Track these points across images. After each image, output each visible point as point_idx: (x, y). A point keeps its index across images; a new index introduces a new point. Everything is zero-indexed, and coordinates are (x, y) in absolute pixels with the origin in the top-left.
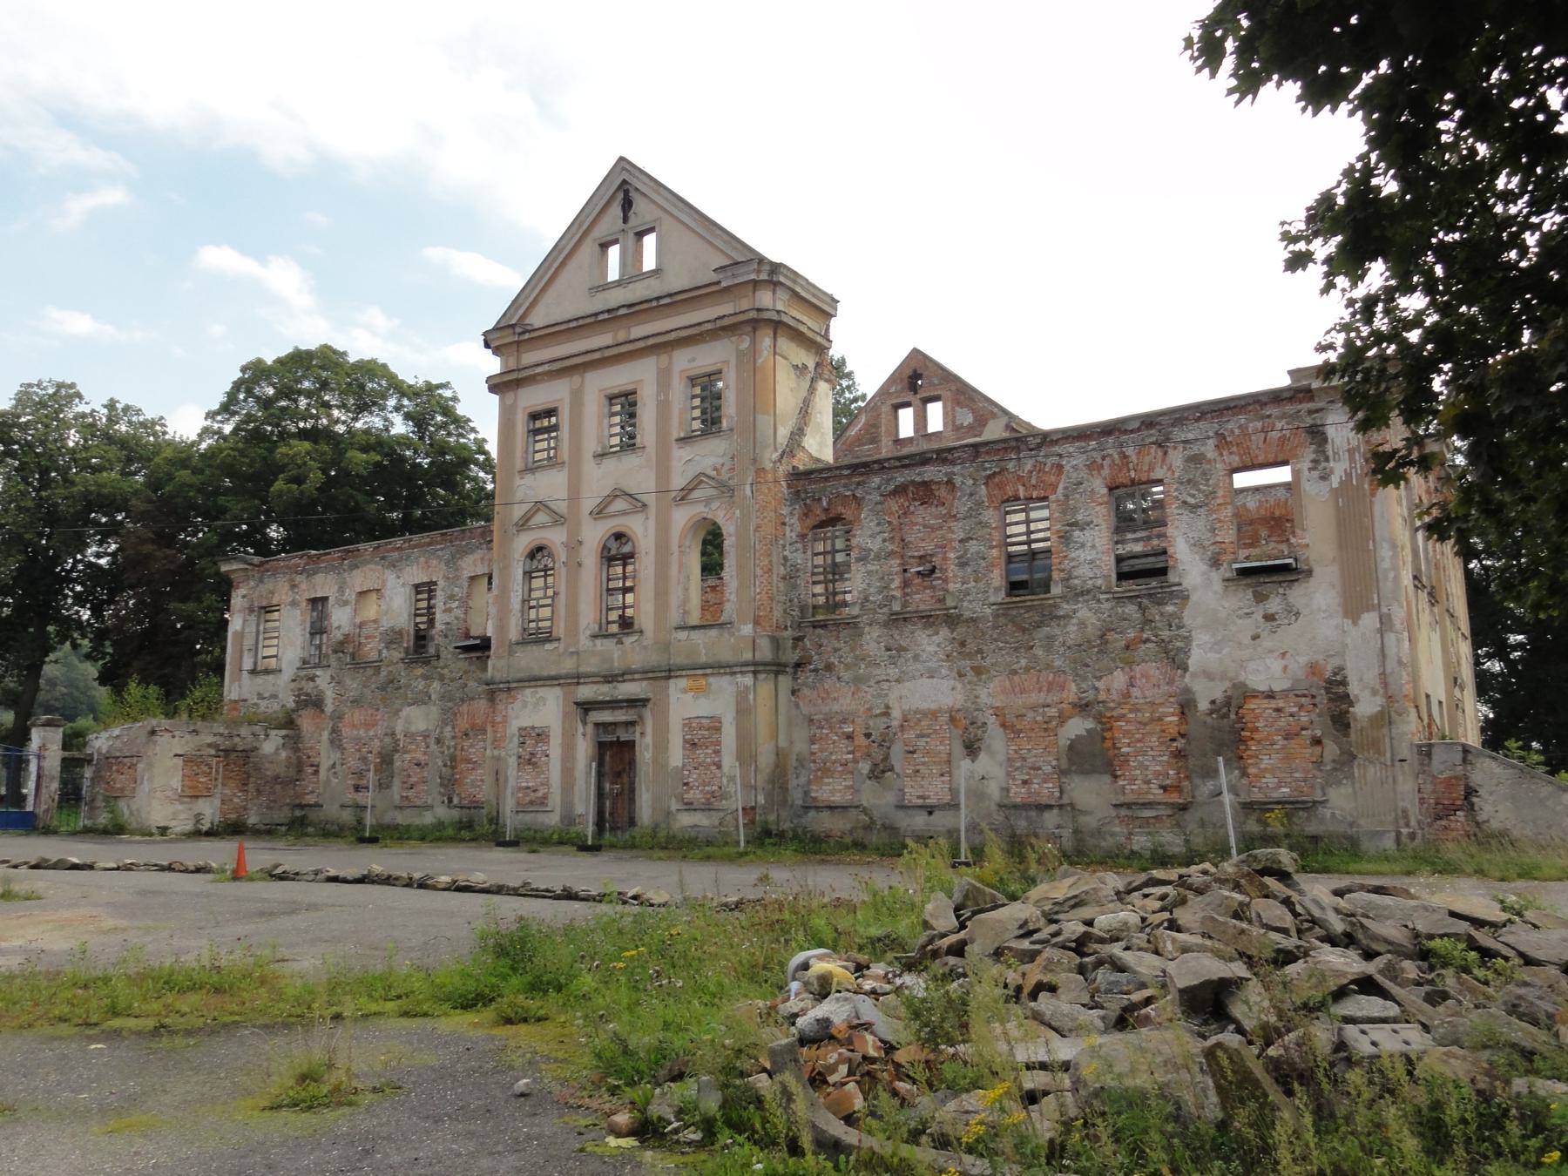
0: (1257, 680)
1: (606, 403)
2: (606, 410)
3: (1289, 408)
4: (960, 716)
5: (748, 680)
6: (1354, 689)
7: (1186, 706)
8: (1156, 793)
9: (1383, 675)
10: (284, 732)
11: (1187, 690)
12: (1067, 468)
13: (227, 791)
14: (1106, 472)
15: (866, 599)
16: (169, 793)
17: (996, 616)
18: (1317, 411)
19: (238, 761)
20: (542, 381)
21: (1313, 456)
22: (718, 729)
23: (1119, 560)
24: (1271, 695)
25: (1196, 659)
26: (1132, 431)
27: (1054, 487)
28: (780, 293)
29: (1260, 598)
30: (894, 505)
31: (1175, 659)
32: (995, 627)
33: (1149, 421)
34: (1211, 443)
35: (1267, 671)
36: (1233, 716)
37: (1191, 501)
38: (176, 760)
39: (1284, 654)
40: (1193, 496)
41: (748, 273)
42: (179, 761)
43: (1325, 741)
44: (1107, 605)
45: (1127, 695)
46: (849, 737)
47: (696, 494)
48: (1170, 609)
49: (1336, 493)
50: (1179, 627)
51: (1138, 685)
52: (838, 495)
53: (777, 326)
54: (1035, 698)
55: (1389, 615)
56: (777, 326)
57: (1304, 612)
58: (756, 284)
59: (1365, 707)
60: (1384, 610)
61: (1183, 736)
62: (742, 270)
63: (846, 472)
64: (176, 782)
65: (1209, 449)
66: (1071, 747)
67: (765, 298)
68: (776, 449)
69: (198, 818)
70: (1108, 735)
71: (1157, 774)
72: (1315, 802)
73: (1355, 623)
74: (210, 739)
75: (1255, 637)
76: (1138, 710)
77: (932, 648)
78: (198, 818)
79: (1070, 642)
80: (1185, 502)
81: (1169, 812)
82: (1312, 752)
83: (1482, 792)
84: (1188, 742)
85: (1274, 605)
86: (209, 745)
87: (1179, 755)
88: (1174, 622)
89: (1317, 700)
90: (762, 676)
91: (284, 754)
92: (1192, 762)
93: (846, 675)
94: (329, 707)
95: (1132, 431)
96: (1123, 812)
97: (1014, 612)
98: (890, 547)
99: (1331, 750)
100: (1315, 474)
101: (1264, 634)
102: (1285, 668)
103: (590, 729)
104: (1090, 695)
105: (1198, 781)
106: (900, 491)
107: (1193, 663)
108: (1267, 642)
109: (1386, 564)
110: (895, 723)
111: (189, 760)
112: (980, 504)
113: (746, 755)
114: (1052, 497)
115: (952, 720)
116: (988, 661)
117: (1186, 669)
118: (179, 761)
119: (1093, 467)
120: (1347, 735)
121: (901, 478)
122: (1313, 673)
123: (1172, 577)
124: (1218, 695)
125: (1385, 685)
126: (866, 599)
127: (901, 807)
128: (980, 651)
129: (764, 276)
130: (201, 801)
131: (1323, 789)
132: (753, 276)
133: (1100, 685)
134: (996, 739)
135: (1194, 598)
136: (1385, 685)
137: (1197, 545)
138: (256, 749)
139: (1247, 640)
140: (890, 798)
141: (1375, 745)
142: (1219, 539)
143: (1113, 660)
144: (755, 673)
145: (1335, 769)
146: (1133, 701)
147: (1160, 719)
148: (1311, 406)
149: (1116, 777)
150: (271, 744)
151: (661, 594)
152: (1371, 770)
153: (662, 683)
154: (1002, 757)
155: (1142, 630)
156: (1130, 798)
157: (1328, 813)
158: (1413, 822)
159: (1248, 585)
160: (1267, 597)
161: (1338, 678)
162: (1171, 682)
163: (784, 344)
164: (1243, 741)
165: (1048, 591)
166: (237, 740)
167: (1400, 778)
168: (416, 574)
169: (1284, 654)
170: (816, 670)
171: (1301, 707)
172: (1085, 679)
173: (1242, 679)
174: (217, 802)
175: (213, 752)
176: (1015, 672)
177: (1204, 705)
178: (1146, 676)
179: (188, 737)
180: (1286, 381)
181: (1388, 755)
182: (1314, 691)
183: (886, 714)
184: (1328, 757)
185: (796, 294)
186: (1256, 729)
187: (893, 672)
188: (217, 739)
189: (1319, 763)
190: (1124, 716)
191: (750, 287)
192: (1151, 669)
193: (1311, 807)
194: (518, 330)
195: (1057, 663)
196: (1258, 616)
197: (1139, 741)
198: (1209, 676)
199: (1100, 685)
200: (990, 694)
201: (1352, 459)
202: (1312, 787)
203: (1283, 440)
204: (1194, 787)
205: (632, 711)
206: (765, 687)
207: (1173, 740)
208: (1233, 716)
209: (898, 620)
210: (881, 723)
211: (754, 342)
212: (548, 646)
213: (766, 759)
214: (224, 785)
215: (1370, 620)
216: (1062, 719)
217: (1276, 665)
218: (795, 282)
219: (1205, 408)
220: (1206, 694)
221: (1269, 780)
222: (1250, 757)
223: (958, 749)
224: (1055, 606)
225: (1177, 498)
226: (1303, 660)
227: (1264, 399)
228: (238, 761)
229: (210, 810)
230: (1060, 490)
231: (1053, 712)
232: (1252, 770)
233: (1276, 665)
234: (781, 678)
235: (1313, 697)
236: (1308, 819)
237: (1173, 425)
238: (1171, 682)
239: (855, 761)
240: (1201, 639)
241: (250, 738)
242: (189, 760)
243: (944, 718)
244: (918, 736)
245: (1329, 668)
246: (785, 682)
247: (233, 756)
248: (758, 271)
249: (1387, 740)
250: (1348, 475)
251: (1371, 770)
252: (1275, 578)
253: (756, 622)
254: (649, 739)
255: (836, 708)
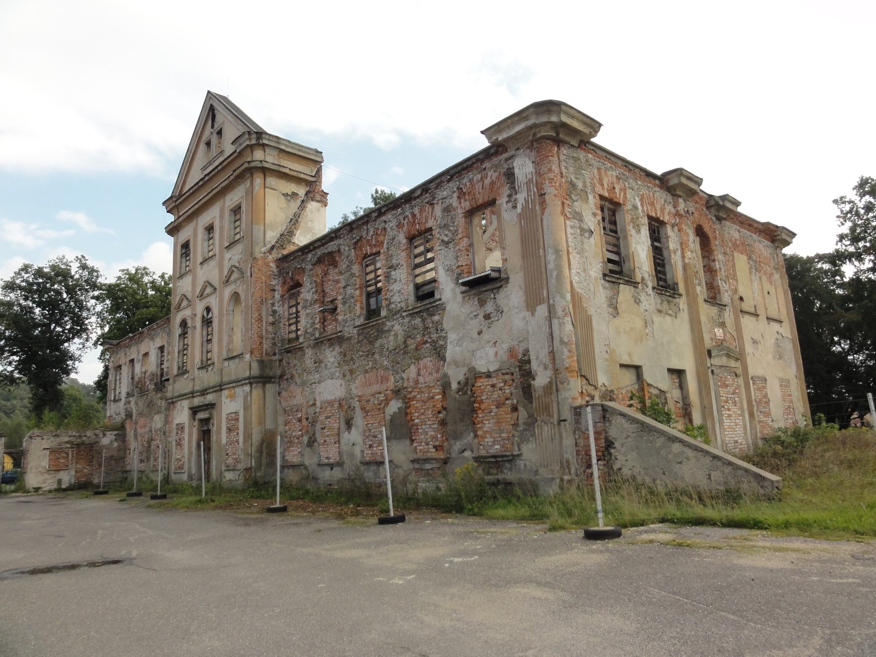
0: (482, 366)
1: (207, 233)
2: (206, 237)
3: (495, 160)
4: (344, 403)
5: (247, 388)
6: (534, 366)
7: (446, 386)
8: (432, 453)
9: (552, 353)
10: (115, 432)
11: (445, 376)
12: (388, 229)
13: (79, 466)
14: (405, 228)
15: (306, 332)
16: (40, 469)
17: (359, 335)
18: (510, 158)
19: (87, 451)
20: (184, 227)
21: (508, 192)
22: (237, 420)
23: (418, 287)
24: (489, 375)
25: (451, 352)
26: (418, 197)
27: (382, 243)
28: (268, 150)
29: (482, 303)
30: (319, 270)
31: (439, 354)
32: (358, 342)
33: (425, 188)
34: (455, 195)
35: (487, 359)
36: (469, 393)
37: (446, 239)
38: (45, 451)
39: (495, 343)
40: (446, 235)
41: (245, 141)
42: (47, 452)
43: (520, 408)
44: (407, 320)
45: (417, 382)
46: (300, 420)
47: (232, 279)
48: (436, 318)
49: (519, 215)
50: (442, 330)
51: (419, 373)
52: (296, 268)
53: (265, 171)
54: (376, 388)
55: (554, 305)
56: (265, 171)
57: (505, 310)
58: (251, 147)
59: (541, 380)
60: (551, 302)
61: (445, 409)
62: (241, 141)
63: (300, 254)
64: (45, 463)
65: (454, 202)
66: (391, 421)
67: (258, 155)
68: (265, 245)
69: (60, 482)
70: (408, 411)
71: (433, 438)
72: (513, 456)
73: (533, 314)
74: (67, 439)
75: (480, 333)
76: (422, 392)
77: (332, 360)
78: (60, 482)
79: (391, 348)
80: (443, 241)
81: (438, 465)
82: (510, 417)
83: (617, 445)
84: (447, 414)
85: (489, 308)
86: (67, 442)
87: (443, 423)
88: (438, 327)
89: (514, 376)
90: (254, 386)
91: (116, 444)
92: (450, 427)
93: (298, 381)
94: (134, 418)
95: (418, 197)
96: (417, 466)
97: (366, 331)
98: (316, 297)
99: (523, 413)
100: (510, 204)
101: (484, 329)
102: (496, 353)
103: (196, 423)
104: (400, 384)
105: (452, 442)
106: (320, 261)
107: (448, 355)
108: (486, 336)
109: (551, 266)
110: (318, 410)
111: (52, 451)
112: (351, 262)
113: (248, 436)
114: (382, 251)
115: (340, 406)
116: (357, 365)
117: (445, 361)
118: (47, 452)
119: (400, 226)
120: (531, 402)
121: (319, 252)
122: (512, 356)
123: (437, 296)
124: (461, 377)
125: (554, 360)
126: (306, 332)
127: (320, 465)
128: (352, 359)
129: (253, 142)
130: (61, 472)
131: (519, 446)
132: (248, 143)
133: (404, 376)
134: (359, 420)
135: (448, 308)
136: (554, 360)
137: (449, 270)
138: (97, 442)
139: (475, 335)
140: (315, 460)
141: (547, 408)
142: (460, 264)
143: (410, 358)
144: (251, 384)
145: (525, 430)
146: (420, 386)
147: (433, 398)
148: (506, 155)
149: (412, 441)
150: (107, 439)
151: (220, 340)
152: (545, 428)
153: (219, 393)
154: (361, 430)
155: (424, 335)
156: (420, 455)
157: (522, 463)
158: (573, 470)
159: (475, 294)
160: (485, 302)
161: (526, 358)
162: (437, 371)
163: (272, 181)
164: (474, 411)
165: (379, 315)
166: (84, 438)
167: (564, 435)
168: (159, 342)
169: (495, 343)
170: (287, 379)
171: (505, 382)
172: (397, 373)
173: (473, 364)
174: (73, 473)
175: (69, 446)
176: (366, 372)
177: (454, 386)
178: (425, 367)
179: (52, 439)
180: (484, 143)
181: (556, 416)
182: (512, 370)
183: (314, 404)
184: (521, 421)
185: (281, 150)
186: (481, 402)
187: (317, 376)
188: (72, 439)
189: (515, 425)
190: (415, 397)
191: (249, 150)
192: (428, 362)
193: (512, 459)
194: (174, 199)
195: (385, 363)
196: (481, 317)
197: (423, 414)
198: (456, 364)
199: (404, 376)
200: (357, 388)
201: (529, 190)
202: (513, 444)
203: (492, 183)
204: (450, 446)
205: (207, 412)
206: (257, 392)
207: (439, 412)
208: (469, 393)
209: (318, 343)
210: (311, 411)
211: (252, 183)
212: (185, 376)
213: (256, 438)
214: (77, 463)
215: (542, 310)
216: (387, 401)
217: (491, 352)
218: (278, 143)
219: (452, 172)
220: (456, 376)
221: (489, 440)
222: (479, 423)
223: (343, 425)
224: (384, 324)
225: (438, 239)
226: (505, 346)
227: (481, 157)
228: (87, 451)
229: (67, 478)
230: (385, 245)
231: (382, 397)
232: (480, 433)
233: (491, 352)
234: (268, 386)
235: (512, 374)
236: (510, 469)
237: (437, 188)
238: (437, 371)
239: (302, 436)
240: (452, 337)
241: (94, 437)
242: (52, 451)
243: (336, 405)
244: (327, 418)
245: (521, 351)
246: (271, 388)
247: (83, 447)
248: (250, 139)
249: (555, 405)
250: (527, 201)
251: (545, 428)
252: (488, 287)
253: (252, 353)
254: (215, 428)
255: (295, 402)
